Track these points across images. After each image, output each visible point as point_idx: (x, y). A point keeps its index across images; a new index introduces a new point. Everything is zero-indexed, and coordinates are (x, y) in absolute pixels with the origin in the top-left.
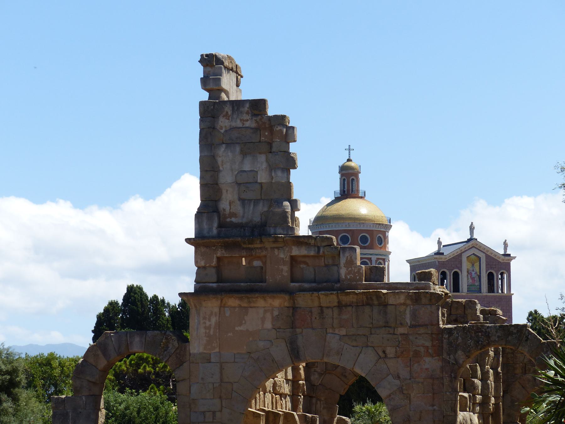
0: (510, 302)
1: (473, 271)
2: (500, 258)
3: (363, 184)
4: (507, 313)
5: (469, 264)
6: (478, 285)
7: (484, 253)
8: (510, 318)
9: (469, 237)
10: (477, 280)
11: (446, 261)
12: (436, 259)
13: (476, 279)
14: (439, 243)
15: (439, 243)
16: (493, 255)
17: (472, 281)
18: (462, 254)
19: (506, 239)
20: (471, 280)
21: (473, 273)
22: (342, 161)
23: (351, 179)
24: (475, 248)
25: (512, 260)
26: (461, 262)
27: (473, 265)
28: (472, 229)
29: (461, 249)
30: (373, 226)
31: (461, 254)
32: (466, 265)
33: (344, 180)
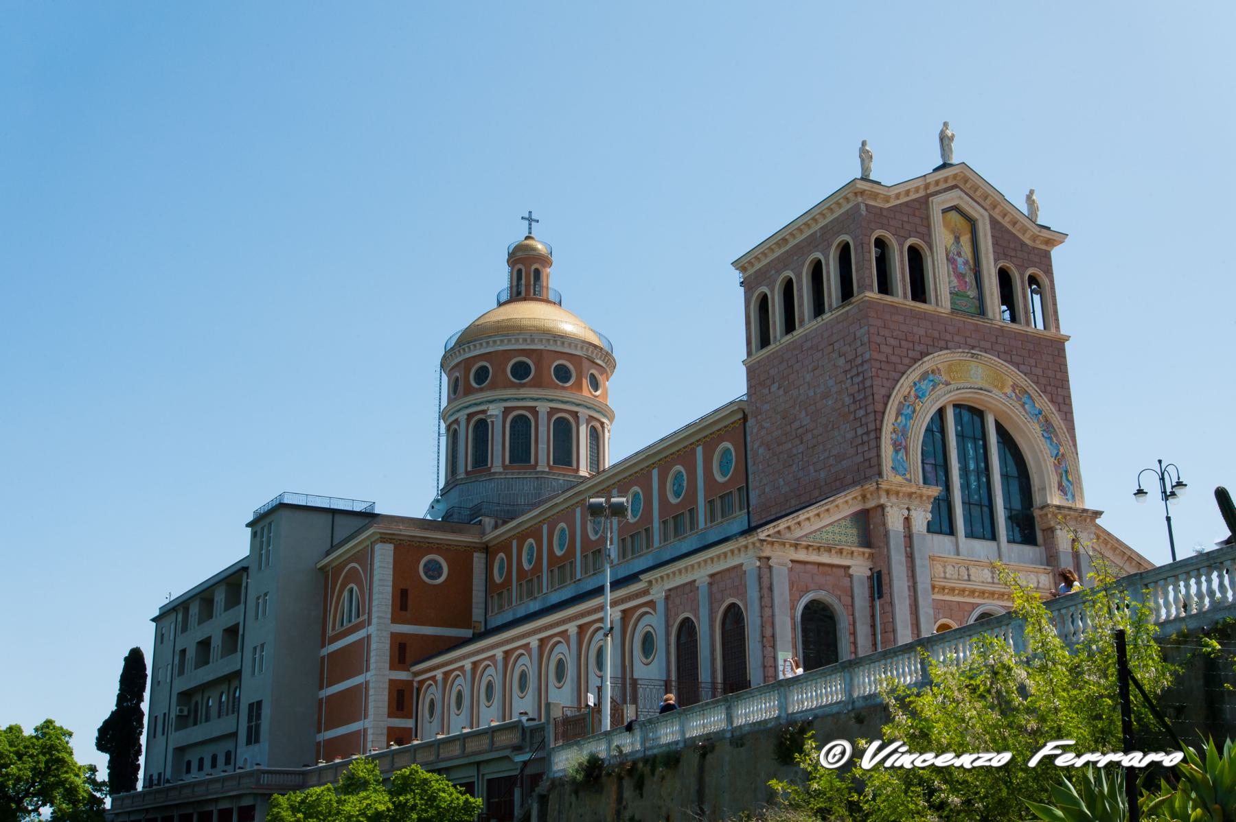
0: (1063, 359)
1: (959, 254)
3: (554, 278)
4: (1057, 388)
6: (973, 298)
8: (1067, 404)
9: (940, 162)
10: (971, 282)
13: (967, 280)
16: (1007, 219)
17: (959, 282)
18: (930, 199)
20: (956, 281)
22: (517, 236)
26: (927, 221)
27: (957, 239)
28: (945, 141)
30: (582, 348)
31: (926, 202)
32: (942, 237)
33: (519, 271)
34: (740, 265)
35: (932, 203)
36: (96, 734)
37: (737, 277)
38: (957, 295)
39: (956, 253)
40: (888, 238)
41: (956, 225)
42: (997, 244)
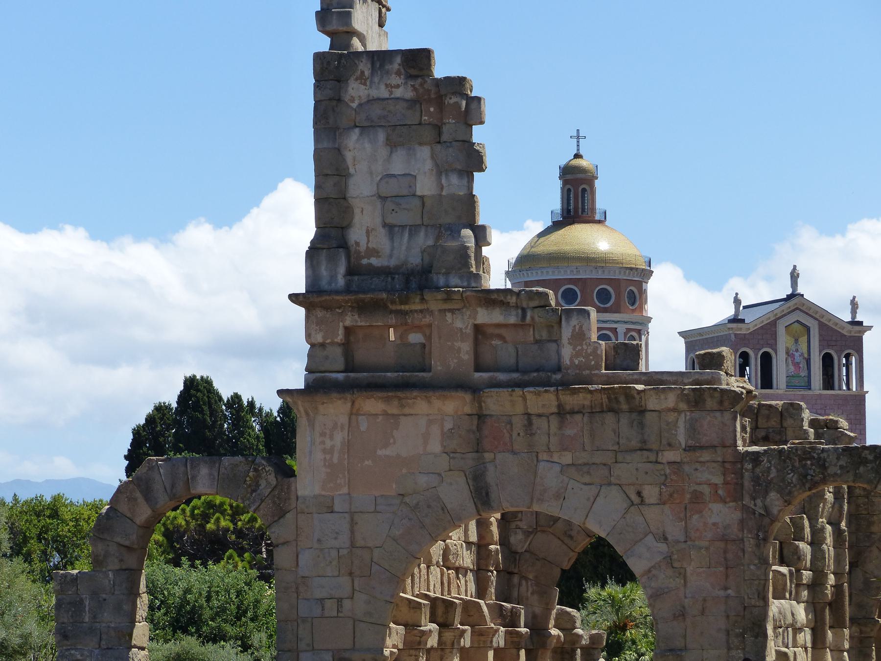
1: (797, 350)
2: (844, 328)
3: (602, 200)
5: (789, 338)
6: (804, 376)
13: (801, 366)
18: (778, 322)
21: (797, 354)
22: (565, 157)
23: (580, 189)
24: (801, 310)
25: (865, 331)
26: (774, 335)
27: (796, 341)
28: (794, 276)
31: (776, 322)
35: (779, 323)
38: (794, 377)
41: (796, 332)
42: (823, 340)
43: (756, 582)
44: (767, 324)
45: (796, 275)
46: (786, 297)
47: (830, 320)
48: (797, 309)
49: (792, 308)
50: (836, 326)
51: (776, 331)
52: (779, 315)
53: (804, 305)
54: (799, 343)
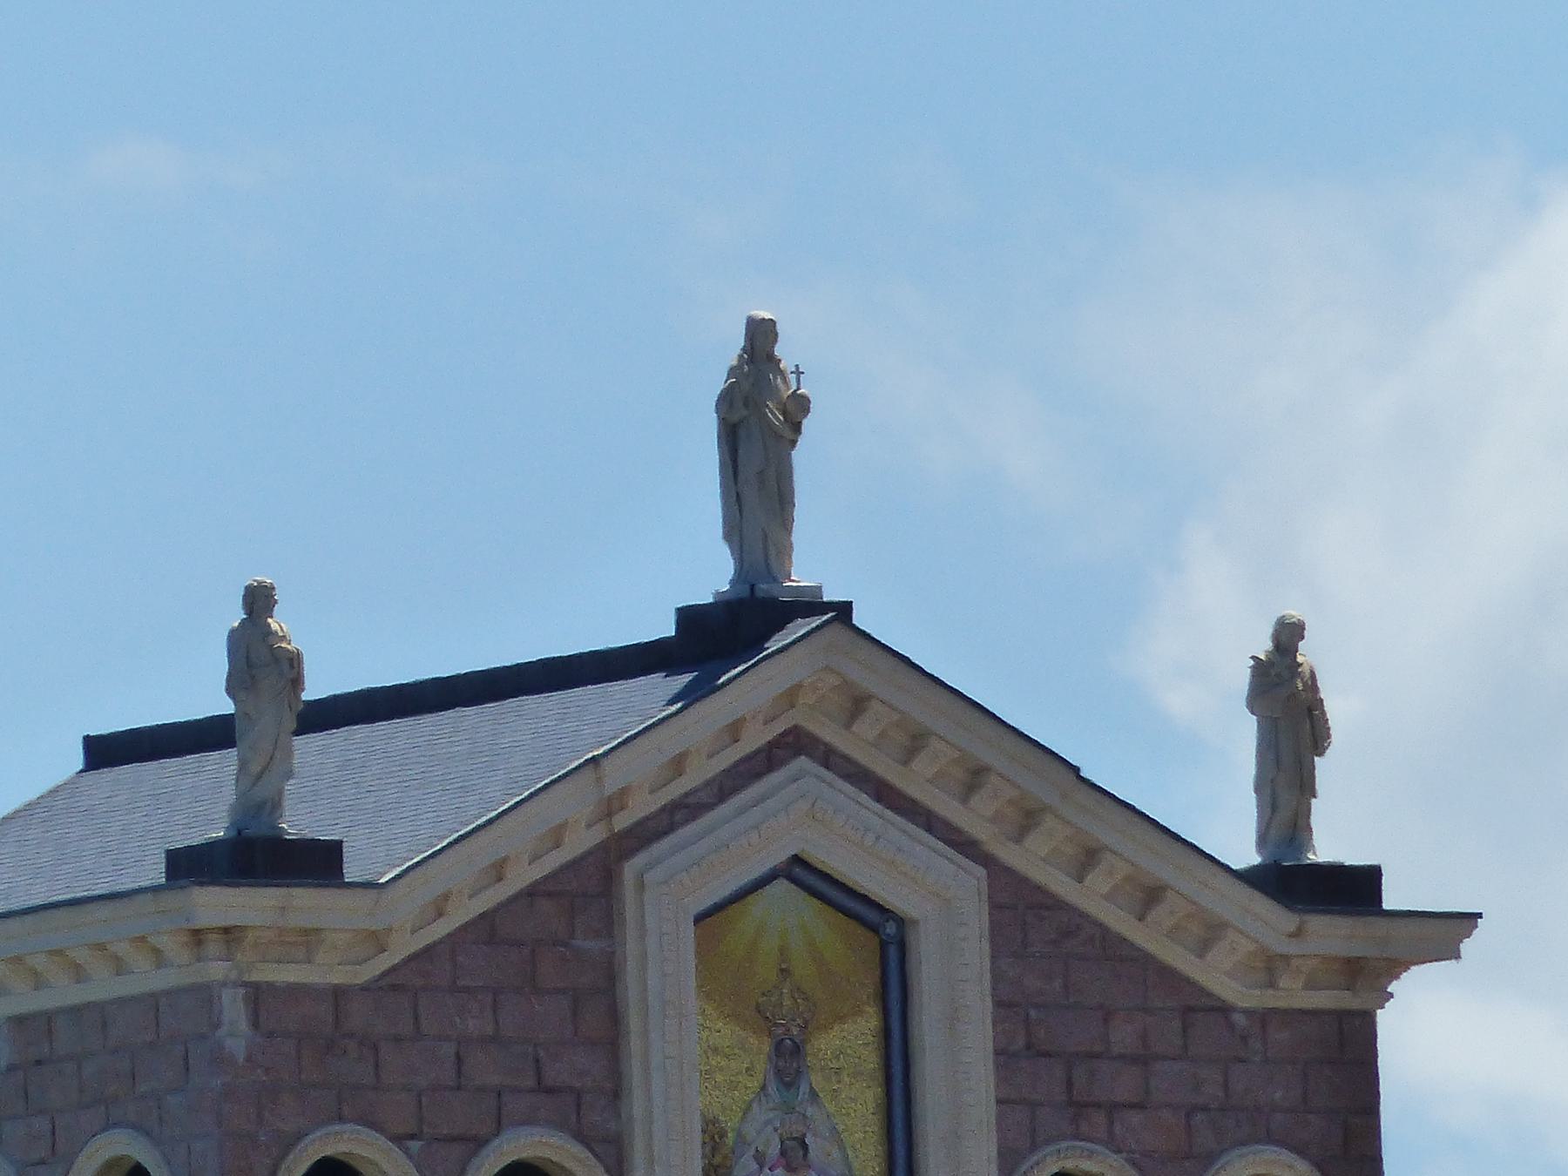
2: (1211, 933)
5: (726, 1033)
7: (965, 846)
11: (365, 988)
12: (214, 946)
14: (803, 373)
15: (803, 373)
18: (630, 868)
19: (1294, 612)
24: (828, 758)
25: (1395, 967)
29: (614, 777)
34: (1458, 957)
35: (641, 886)
36: (1328, 716)
37: (1466, 946)
39: (774, 1150)
40: (371, 1162)
41: (785, 972)
42: (1034, 1050)
43: (770, 1129)
44: (532, 893)
45: (776, 417)
46: (671, 631)
47: (1151, 896)
48: (794, 743)
49: (755, 739)
50: (1203, 948)
51: (610, 973)
52: (642, 806)
53: (858, 704)
54: (816, 1079)
